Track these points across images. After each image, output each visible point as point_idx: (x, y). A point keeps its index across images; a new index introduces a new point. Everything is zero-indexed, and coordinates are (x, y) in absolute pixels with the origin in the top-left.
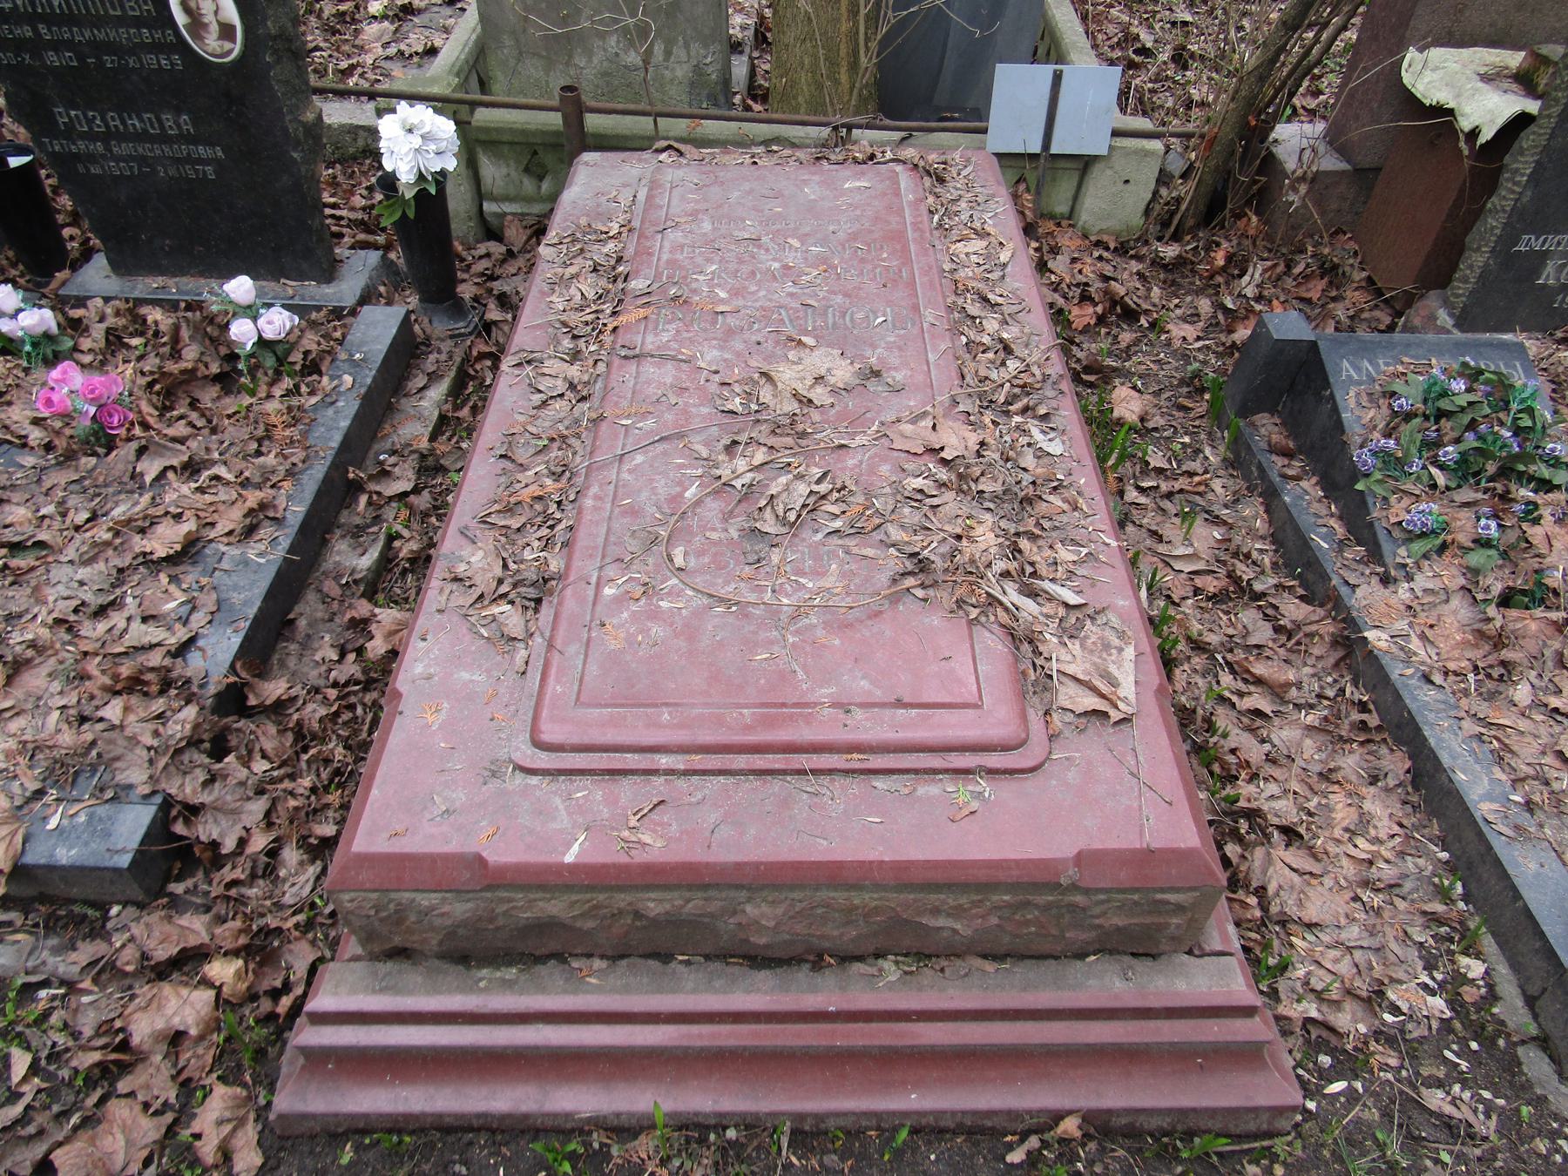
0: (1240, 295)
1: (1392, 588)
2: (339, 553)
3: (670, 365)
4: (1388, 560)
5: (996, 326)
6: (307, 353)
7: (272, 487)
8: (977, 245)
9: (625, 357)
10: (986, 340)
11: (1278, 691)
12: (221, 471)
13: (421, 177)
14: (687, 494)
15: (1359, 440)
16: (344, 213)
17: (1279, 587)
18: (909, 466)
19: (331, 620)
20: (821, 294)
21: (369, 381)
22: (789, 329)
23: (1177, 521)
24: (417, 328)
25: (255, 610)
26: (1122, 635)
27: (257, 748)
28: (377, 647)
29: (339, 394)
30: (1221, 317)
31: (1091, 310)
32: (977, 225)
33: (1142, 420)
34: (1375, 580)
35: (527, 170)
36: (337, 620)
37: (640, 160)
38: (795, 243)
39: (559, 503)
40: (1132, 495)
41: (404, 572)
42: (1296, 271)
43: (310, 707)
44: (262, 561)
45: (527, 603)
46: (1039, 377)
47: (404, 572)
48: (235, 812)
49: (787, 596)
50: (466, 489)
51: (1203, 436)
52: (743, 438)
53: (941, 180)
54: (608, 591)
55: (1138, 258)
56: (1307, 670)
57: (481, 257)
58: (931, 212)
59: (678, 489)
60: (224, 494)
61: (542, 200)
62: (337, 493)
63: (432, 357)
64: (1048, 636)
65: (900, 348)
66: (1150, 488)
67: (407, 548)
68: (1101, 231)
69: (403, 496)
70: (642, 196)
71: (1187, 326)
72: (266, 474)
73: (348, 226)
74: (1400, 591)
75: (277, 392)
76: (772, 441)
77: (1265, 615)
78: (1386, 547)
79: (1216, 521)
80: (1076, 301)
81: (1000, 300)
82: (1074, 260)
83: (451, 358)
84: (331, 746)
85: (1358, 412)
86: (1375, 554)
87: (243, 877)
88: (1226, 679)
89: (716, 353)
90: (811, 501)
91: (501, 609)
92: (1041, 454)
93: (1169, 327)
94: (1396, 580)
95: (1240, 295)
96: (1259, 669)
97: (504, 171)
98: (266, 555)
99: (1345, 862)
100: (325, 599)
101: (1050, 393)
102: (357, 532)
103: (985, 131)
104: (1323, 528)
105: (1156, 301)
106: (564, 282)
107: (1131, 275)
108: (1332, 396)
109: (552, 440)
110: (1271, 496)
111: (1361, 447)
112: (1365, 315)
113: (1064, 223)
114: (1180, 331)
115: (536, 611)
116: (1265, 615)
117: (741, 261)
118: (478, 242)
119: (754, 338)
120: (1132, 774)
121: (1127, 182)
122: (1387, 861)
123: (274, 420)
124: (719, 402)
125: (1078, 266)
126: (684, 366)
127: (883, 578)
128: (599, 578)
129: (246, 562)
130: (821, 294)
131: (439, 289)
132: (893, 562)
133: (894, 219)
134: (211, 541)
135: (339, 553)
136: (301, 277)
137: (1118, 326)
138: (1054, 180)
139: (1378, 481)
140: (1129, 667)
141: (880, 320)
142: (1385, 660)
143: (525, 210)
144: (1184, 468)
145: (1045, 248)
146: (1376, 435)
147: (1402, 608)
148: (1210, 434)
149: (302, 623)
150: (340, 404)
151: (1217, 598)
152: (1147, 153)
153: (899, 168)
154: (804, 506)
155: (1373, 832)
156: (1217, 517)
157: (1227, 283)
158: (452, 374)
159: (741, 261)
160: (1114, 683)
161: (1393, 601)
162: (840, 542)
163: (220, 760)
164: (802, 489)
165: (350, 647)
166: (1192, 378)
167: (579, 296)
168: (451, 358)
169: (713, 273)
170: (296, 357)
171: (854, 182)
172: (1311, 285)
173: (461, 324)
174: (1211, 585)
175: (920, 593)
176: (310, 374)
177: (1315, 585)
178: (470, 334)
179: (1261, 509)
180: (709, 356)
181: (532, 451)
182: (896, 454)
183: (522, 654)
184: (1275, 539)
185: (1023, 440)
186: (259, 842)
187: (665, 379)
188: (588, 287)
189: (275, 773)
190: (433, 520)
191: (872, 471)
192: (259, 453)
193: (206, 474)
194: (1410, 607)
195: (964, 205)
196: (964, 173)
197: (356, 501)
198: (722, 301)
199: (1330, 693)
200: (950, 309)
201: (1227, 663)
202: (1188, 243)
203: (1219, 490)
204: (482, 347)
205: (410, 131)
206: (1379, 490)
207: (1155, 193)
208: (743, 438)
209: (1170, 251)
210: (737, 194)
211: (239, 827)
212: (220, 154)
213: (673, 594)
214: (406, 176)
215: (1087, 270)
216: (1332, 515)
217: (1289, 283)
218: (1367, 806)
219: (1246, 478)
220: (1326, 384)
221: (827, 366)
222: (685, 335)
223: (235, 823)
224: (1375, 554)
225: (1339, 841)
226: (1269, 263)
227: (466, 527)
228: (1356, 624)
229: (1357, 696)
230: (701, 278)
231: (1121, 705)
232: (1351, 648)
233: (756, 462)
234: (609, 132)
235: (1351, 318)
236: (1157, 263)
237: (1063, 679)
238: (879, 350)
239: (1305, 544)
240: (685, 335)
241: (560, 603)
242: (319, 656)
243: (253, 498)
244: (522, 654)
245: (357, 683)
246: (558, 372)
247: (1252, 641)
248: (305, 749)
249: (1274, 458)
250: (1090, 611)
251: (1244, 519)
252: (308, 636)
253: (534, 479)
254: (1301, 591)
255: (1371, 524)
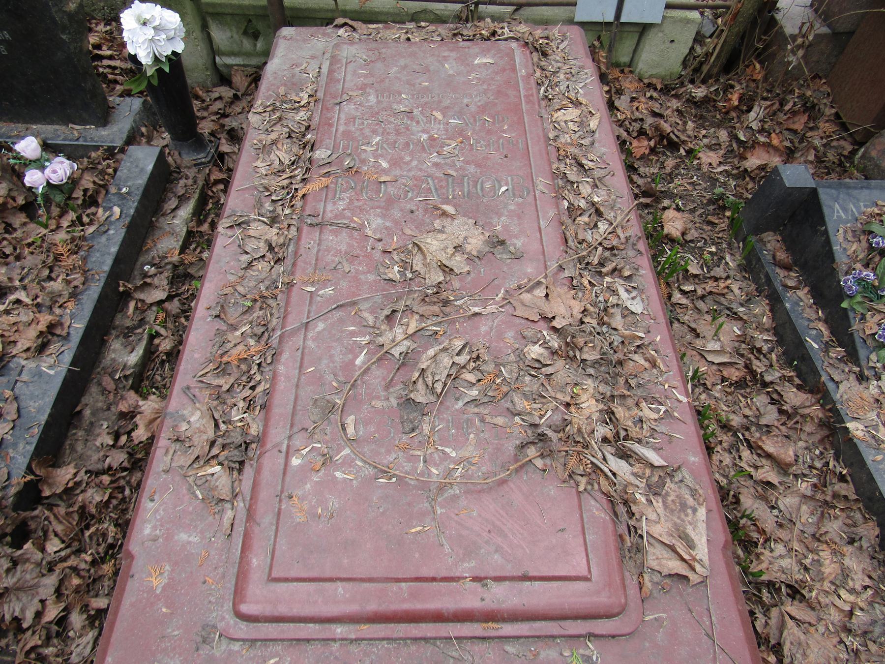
0: (747, 127)
1: (864, 384)
2: (114, 351)
3: (344, 233)
4: (863, 363)
5: (589, 190)
6: (85, 191)
7: (60, 307)
8: (573, 113)
9: (311, 225)
10: (583, 204)
11: (783, 467)
12: (22, 295)
13: (156, 59)
14: (358, 362)
15: (844, 268)
16: (117, 63)
17: (783, 378)
18: (528, 333)
19: (109, 409)
20: (459, 164)
21: (132, 211)
22: (434, 198)
23: (708, 318)
24: (170, 159)
25: (46, 416)
26: (694, 493)
27: (51, 529)
28: (141, 434)
29: (111, 223)
30: (734, 145)
31: (646, 143)
32: (572, 95)
33: (683, 234)
34: (852, 377)
35: (245, 33)
36: (113, 409)
37: (324, 35)
38: (438, 115)
39: (259, 365)
40: (677, 297)
41: (163, 362)
42: (787, 108)
43: (90, 491)
44: (52, 372)
45: (233, 465)
46: (623, 240)
47: (163, 362)
48: (36, 586)
49: (436, 466)
50: (212, 267)
51: (724, 246)
52: (401, 306)
53: (545, 54)
54: (295, 461)
55: (676, 96)
56: (801, 444)
57: (216, 99)
58: (538, 84)
59: (350, 356)
60: (24, 316)
61: (258, 55)
62: (111, 302)
63: (182, 182)
64: (638, 496)
65: (519, 217)
66: (689, 292)
67: (165, 345)
68: (651, 76)
69: (160, 303)
70: (325, 69)
71: (711, 154)
72: (54, 298)
73: (121, 74)
74: (871, 387)
75: (65, 223)
76: (422, 309)
77: (772, 399)
78: (862, 353)
79: (735, 316)
80: (635, 134)
81: (591, 164)
82: (633, 99)
83: (195, 182)
84: (105, 526)
85: (845, 247)
86: (852, 356)
87: (40, 643)
88: (746, 453)
89: (379, 221)
90: (453, 372)
91: (211, 470)
92: (627, 313)
93: (700, 155)
94: (868, 379)
95: (747, 127)
96: (769, 446)
97: (229, 34)
98: (55, 367)
99: (832, 610)
100: (104, 391)
101: (631, 253)
102: (127, 333)
103: (575, 5)
104: (815, 333)
105: (691, 133)
106: (265, 149)
107: (673, 112)
108: (826, 232)
109: (255, 301)
110: (775, 301)
111: (847, 273)
112: (834, 144)
113: (626, 70)
114: (709, 158)
115: (240, 471)
116: (772, 399)
117: (398, 133)
118: (215, 86)
119: (408, 206)
120: (708, 635)
121: (672, 41)
122: (862, 609)
123: (61, 250)
124: (382, 270)
125: (636, 104)
126: (355, 234)
127: (510, 447)
128: (288, 447)
129: (40, 374)
130: (459, 164)
131: (186, 132)
132: (518, 430)
133: (512, 93)
134: (14, 356)
135: (114, 351)
136: (83, 122)
137: (664, 154)
138: (621, 39)
139: (859, 303)
140: (702, 527)
141: (504, 189)
142: (862, 448)
143: (246, 62)
144: (712, 273)
145: (613, 90)
146: (858, 266)
147: (872, 400)
148: (729, 244)
149: (87, 412)
150: (111, 232)
151: (740, 384)
152: (688, 21)
153: (514, 45)
154: (449, 376)
155: (851, 583)
156: (735, 313)
157: (738, 117)
158: (196, 196)
159: (398, 133)
160: (691, 545)
161: (865, 394)
162: (476, 410)
163: (20, 547)
164: (446, 361)
165: (122, 431)
166: (717, 200)
167: (277, 162)
168: (195, 182)
169: (377, 144)
170: (78, 194)
171: (483, 58)
172: (796, 119)
173: (202, 155)
174: (734, 374)
175: (539, 463)
176: (90, 207)
177: (810, 380)
178: (209, 162)
179: (767, 308)
180: (374, 224)
181: (240, 310)
182: (518, 321)
183: (229, 514)
184: (776, 331)
185: (613, 300)
186: (52, 613)
187: (342, 247)
188: (283, 154)
189: (63, 554)
190: (183, 320)
191: (500, 337)
192: (50, 278)
193: (12, 297)
194: (878, 401)
195: (562, 76)
196: (562, 47)
197: (126, 305)
198: (385, 171)
199: (818, 464)
200: (554, 175)
201: (746, 440)
202: (712, 85)
203: (737, 291)
204: (216, 175)
205: (145, 24)
206: (859, 309)
207: (692, 49)
208: (401, 306)
209: (700, 92)
210: (395, 69)
211: (36, 600)
212: (7, 36)
213: (348, 463)
214: (145, 59)
215: (642, 107)
216: (819, 319)
217: (782, 117)
218: (847, 562)
219: (756, 280)
220: (822, 220)
221: (464, 234)
222: (356, 204)
223: (33, 596)
224: (852, 356)
225: (827, 592)
226: (769, 103)
227: (188, 388)
228: (839, 415)
229: (838, 469)
230: (369, 149)
231: (698, 567)
232: (834, 431)
233: (411, 331)
234: (303, 6)
235: (824, 146)
236: (691, 101)
237: (652, 541)
238: (503, 218)
239: (801, 344)
240: (356, 204)
241: (258, 471)
242: (97, 445)
243: (45, 319)
244: (229, 514)
245: (125, 469)
246: (262, 232)
247: (763, 421)
248: (88, 527)
249: (778, 270)
250: (669, 470)
251: (755, 316)
252: (92, 423)
253: (241, 343)
254: (797, 381)
255: (852, 334)
